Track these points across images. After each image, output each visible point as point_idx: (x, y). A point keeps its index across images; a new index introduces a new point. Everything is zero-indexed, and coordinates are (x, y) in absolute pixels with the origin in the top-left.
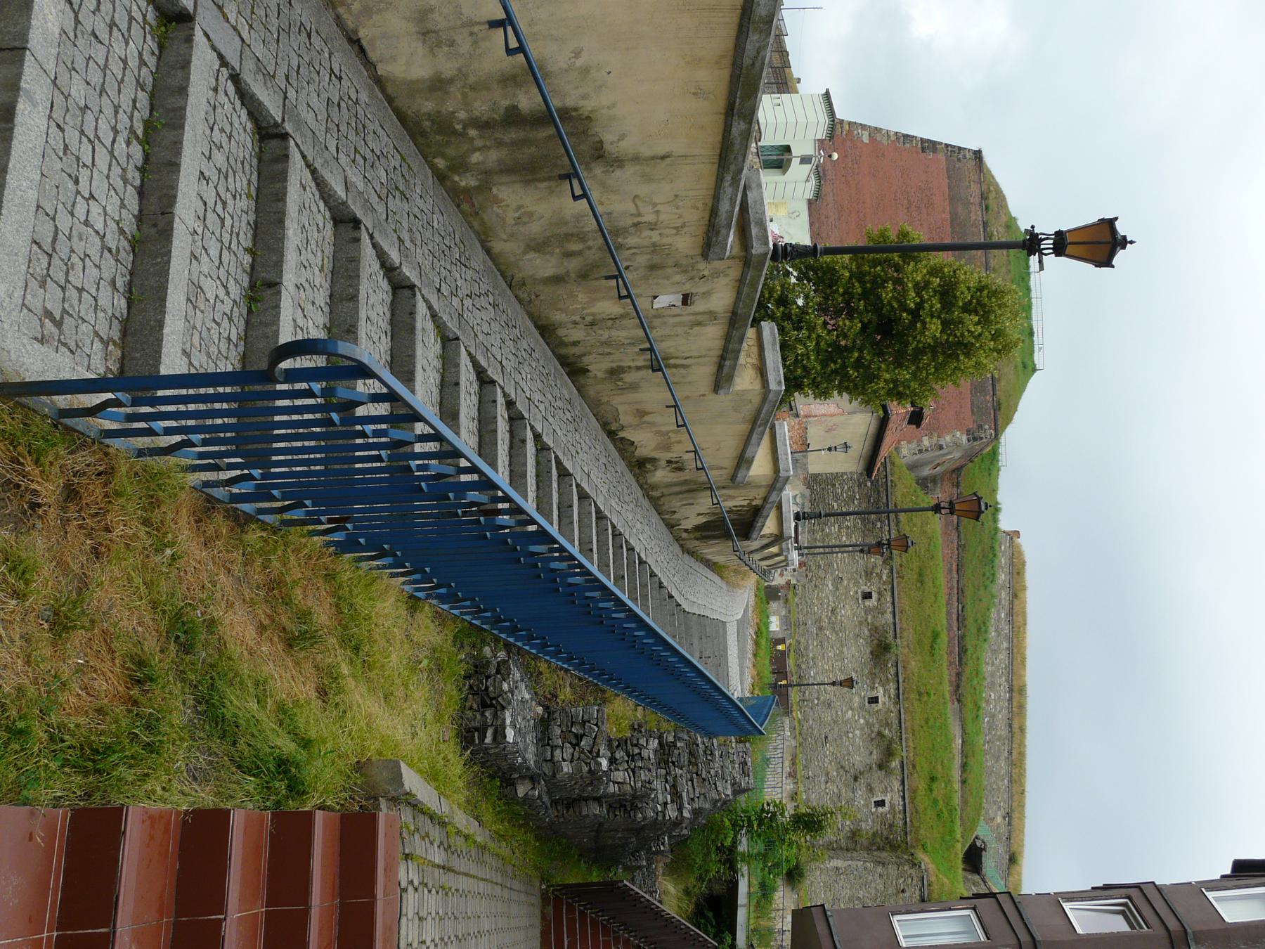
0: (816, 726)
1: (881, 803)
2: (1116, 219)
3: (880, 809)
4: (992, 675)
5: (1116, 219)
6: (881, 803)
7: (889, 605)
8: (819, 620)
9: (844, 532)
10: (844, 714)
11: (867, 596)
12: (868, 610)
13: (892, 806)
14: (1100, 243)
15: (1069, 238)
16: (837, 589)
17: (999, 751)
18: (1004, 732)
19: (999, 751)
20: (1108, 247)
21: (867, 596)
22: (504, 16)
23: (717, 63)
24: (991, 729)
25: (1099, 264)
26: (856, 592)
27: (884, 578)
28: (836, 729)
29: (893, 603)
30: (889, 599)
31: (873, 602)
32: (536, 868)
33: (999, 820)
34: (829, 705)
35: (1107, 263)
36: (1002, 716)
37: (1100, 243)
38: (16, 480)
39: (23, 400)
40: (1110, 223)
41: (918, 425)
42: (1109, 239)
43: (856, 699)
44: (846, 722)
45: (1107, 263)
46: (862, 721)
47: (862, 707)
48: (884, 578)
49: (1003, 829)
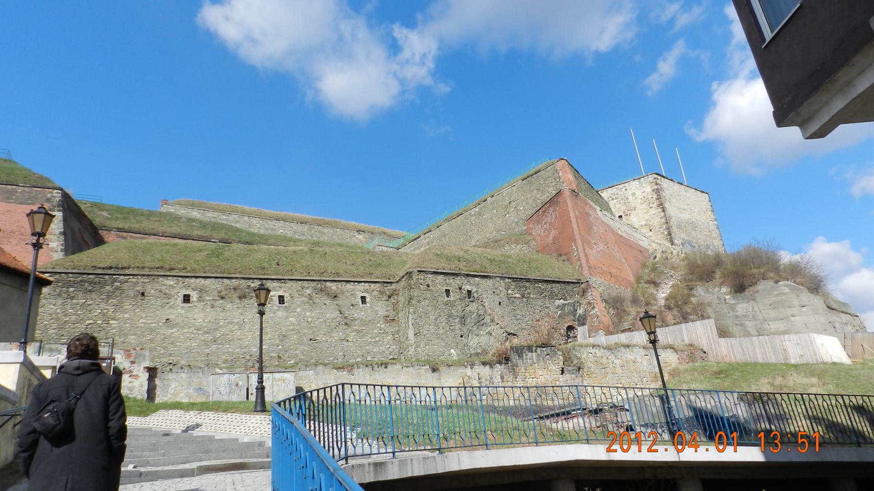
0: (301, 348)
1: (363, 299)
3: (368, 300)
4: (267, 229)
6: (363, 299)
7: (198, 280)
8: (206, 343)
9: (119, 315)
10: (292, 324)
11: (187, 299)
12: (200, 299)
13: (367, 291)
16: (177, 324)
17: (319, 231)
18: (306, 227)
19: (319, 231)
21: (187, 299)
22: (158, 400)
23: (820, 281)
24: (303, 234)
26: (183, 308)
28: (306, 331)
29: (197, 277)
30: (193, 280)
31: (194, 296)
33: (361, 237)
34: (284, 336)
36: (296, 227)
38: (294, 419)
41: (185, 296)
46: (299, 310)
48: (172, 283)
49: (367, 235)
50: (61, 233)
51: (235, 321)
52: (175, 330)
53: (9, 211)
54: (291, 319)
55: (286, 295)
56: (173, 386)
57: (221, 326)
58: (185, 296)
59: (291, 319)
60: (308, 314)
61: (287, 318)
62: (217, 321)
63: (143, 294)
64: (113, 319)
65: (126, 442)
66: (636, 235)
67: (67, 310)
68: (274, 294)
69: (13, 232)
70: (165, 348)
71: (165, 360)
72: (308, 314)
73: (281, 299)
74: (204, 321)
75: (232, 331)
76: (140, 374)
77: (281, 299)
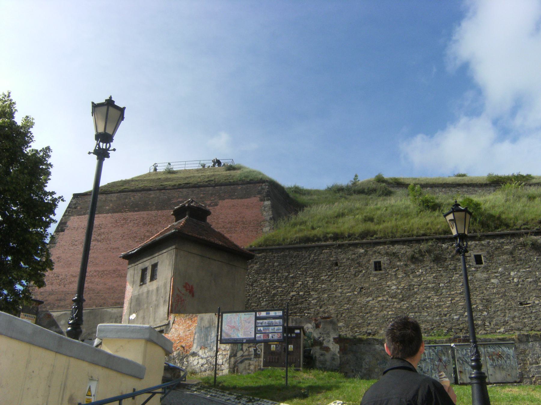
2: (93, 103)
5: (93, 103)
11: (378, 266)
14: (90, 153)
15: (101, 130)
20: (111, 109)
25: (122, 117)
26: (375, 276)
27: (362, 251)
31: (384, 260)
32: (380, 196)
34: (487, 300)
35: (122, 111)
37: (90, 153)
39: (128, 385)
40: (95, 107)
41: (376, 263)
42: (105, 108)
43: (478, 275)
44: (503, 285)
45: (122, 111)
47: (486, 269)
50: (271, 219)
51: (430, 286)
52: (370, 298)
53: (233, 206)
54: (493, 281)
55: (483, 254)
56: (367, 360)
57: (416, 293)
58: (376, 263)
59: (493, 281)
60: (512, 274)
61: (488, 280)
62: (410, 287)
63: (336, 264)
64: (313, 290)
65: (525, 175)
66: (198, 376)
67: (274, 283)
68: (472, 254)
69: (237, 222)
70: (363, 317)
71: (365, 330)
72: (512, 274)
73: (478, 260)
74: (398, 288)
75: (429, 298)
76: (331, 346)
77: (478, 260)
